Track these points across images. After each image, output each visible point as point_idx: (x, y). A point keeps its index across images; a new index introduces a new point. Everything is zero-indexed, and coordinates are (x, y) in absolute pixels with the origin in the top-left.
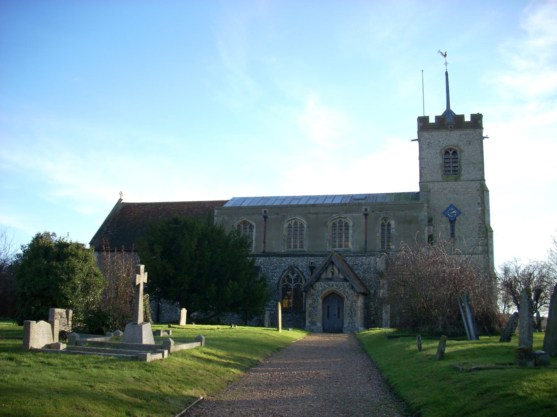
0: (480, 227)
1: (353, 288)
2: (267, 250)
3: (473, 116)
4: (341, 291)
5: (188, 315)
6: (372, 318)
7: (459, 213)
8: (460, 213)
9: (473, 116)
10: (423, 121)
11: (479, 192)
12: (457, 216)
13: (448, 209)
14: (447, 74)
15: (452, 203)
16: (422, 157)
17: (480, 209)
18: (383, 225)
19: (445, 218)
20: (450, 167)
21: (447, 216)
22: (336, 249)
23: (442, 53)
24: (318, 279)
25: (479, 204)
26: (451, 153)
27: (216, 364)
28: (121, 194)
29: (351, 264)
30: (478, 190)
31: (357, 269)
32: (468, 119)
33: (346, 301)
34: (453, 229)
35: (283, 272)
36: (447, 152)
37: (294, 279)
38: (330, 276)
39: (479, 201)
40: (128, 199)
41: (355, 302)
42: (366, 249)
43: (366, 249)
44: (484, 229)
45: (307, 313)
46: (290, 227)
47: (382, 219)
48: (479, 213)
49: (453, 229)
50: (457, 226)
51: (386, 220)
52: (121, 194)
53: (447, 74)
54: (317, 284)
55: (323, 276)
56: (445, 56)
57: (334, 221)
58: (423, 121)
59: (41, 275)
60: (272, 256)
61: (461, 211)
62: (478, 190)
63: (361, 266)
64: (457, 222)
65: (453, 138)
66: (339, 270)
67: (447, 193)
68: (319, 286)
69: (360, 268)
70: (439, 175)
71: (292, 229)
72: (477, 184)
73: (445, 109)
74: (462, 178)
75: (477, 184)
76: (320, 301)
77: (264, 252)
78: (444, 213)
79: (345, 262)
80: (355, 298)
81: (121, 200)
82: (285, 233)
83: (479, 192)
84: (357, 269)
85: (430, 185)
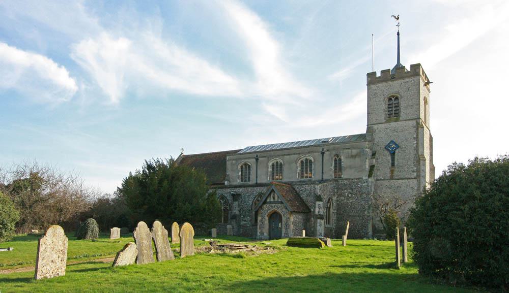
0: (415, 157)
1: (287, 209)
2: (258, 182)
3: (412, 66)
4: (280, 211)
5: (306, 233)
6: (312, 229)
7: (397, 146)
8: (399, 146)
9: (412, 66)
10: (371, 76)
11: (415, 129)
12: (395, 149)
13: (389, 144)
14: (398, 34)
15: (392, 139)
16: (418, 107)
17: (416, 142)
18: (336, 160)
19: (386, 152)
20: (392, 111)
21: (388, 150)
22: (303, 179)
23: (395, 17)
24: (265, 202)
25: (414, 138)
26: (393, 99)
27: (369, 267)
28: (182, 149)
29: (298, 190)
30: (414, 127)
31: (302, 194)
32: (378, 75)
33: (283, 217)
34: (393, 159)
35: (255, 198)
36: (390, 99)
37: (224, 203)
38: (272, 200)
39: (415, 136)
40: (186, 153)
41: (289, 218)
42: (323, 178)
43: (323, 178)
44: (418, 158)
45: (258, 227)
46: (273, 165)
47: (335, 156)
48: (415, 146)
49: (393, 159)
50: (396, 157)
51: (338, 156)
52: (182, 149)
53: (398, 34)
54: (265, 206)
55: (268, 200)
56: (398, 19)
57: (301, 159)
58: (371, 76)
59: (31, 206)
60: (262, 186)
61: (400, 145)
62: (414, 127)
63: (305, 192)
64: (396, 154)
65: (395, 86)
66: (278, 197)
67: (386, 132)
68: (266, 207)
69: (304, 193)
70: (382, 117)
71: (275, 167)
72: (414, 122)
73: (396, 63)
74: (401, 119)
75: (414, 122)
76: (267, 218)
77: (257, 183)
78: (386, 148)
79: (294, 189)
80: (288, 216)
81: (182, 153)
82: (270, 169)
83: (415, 129)
84: (302, 194)
85: (375, 127)
